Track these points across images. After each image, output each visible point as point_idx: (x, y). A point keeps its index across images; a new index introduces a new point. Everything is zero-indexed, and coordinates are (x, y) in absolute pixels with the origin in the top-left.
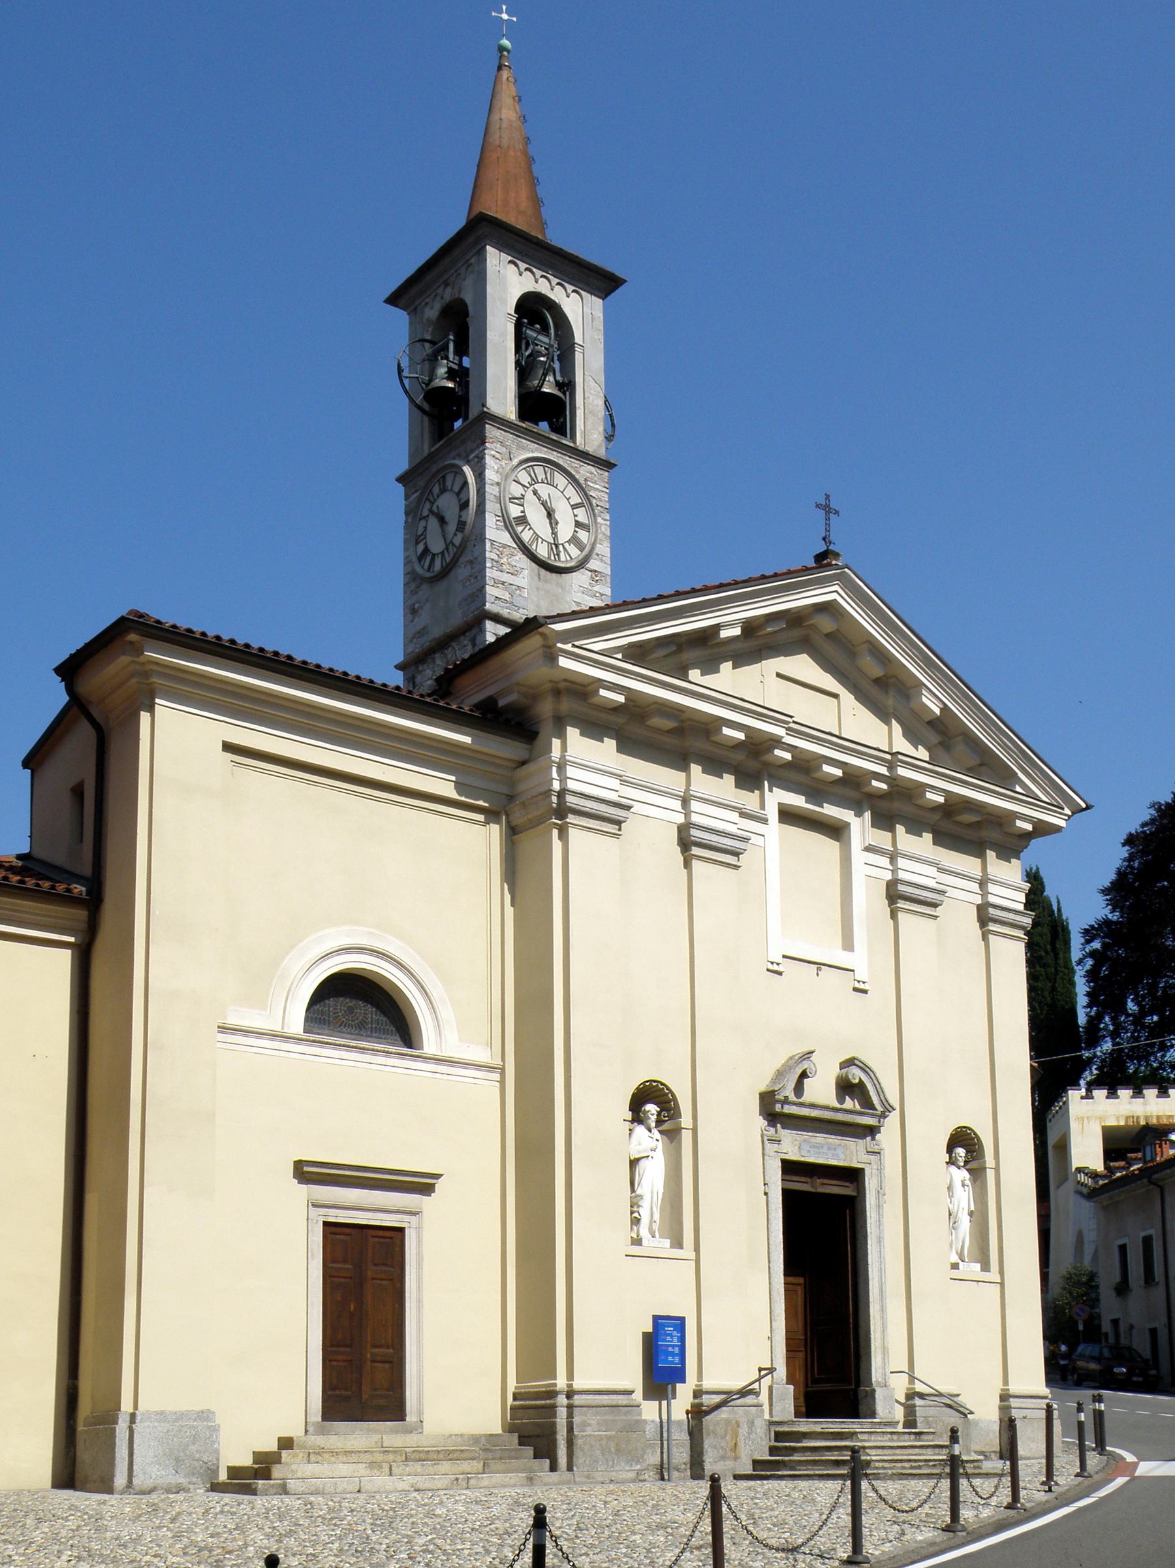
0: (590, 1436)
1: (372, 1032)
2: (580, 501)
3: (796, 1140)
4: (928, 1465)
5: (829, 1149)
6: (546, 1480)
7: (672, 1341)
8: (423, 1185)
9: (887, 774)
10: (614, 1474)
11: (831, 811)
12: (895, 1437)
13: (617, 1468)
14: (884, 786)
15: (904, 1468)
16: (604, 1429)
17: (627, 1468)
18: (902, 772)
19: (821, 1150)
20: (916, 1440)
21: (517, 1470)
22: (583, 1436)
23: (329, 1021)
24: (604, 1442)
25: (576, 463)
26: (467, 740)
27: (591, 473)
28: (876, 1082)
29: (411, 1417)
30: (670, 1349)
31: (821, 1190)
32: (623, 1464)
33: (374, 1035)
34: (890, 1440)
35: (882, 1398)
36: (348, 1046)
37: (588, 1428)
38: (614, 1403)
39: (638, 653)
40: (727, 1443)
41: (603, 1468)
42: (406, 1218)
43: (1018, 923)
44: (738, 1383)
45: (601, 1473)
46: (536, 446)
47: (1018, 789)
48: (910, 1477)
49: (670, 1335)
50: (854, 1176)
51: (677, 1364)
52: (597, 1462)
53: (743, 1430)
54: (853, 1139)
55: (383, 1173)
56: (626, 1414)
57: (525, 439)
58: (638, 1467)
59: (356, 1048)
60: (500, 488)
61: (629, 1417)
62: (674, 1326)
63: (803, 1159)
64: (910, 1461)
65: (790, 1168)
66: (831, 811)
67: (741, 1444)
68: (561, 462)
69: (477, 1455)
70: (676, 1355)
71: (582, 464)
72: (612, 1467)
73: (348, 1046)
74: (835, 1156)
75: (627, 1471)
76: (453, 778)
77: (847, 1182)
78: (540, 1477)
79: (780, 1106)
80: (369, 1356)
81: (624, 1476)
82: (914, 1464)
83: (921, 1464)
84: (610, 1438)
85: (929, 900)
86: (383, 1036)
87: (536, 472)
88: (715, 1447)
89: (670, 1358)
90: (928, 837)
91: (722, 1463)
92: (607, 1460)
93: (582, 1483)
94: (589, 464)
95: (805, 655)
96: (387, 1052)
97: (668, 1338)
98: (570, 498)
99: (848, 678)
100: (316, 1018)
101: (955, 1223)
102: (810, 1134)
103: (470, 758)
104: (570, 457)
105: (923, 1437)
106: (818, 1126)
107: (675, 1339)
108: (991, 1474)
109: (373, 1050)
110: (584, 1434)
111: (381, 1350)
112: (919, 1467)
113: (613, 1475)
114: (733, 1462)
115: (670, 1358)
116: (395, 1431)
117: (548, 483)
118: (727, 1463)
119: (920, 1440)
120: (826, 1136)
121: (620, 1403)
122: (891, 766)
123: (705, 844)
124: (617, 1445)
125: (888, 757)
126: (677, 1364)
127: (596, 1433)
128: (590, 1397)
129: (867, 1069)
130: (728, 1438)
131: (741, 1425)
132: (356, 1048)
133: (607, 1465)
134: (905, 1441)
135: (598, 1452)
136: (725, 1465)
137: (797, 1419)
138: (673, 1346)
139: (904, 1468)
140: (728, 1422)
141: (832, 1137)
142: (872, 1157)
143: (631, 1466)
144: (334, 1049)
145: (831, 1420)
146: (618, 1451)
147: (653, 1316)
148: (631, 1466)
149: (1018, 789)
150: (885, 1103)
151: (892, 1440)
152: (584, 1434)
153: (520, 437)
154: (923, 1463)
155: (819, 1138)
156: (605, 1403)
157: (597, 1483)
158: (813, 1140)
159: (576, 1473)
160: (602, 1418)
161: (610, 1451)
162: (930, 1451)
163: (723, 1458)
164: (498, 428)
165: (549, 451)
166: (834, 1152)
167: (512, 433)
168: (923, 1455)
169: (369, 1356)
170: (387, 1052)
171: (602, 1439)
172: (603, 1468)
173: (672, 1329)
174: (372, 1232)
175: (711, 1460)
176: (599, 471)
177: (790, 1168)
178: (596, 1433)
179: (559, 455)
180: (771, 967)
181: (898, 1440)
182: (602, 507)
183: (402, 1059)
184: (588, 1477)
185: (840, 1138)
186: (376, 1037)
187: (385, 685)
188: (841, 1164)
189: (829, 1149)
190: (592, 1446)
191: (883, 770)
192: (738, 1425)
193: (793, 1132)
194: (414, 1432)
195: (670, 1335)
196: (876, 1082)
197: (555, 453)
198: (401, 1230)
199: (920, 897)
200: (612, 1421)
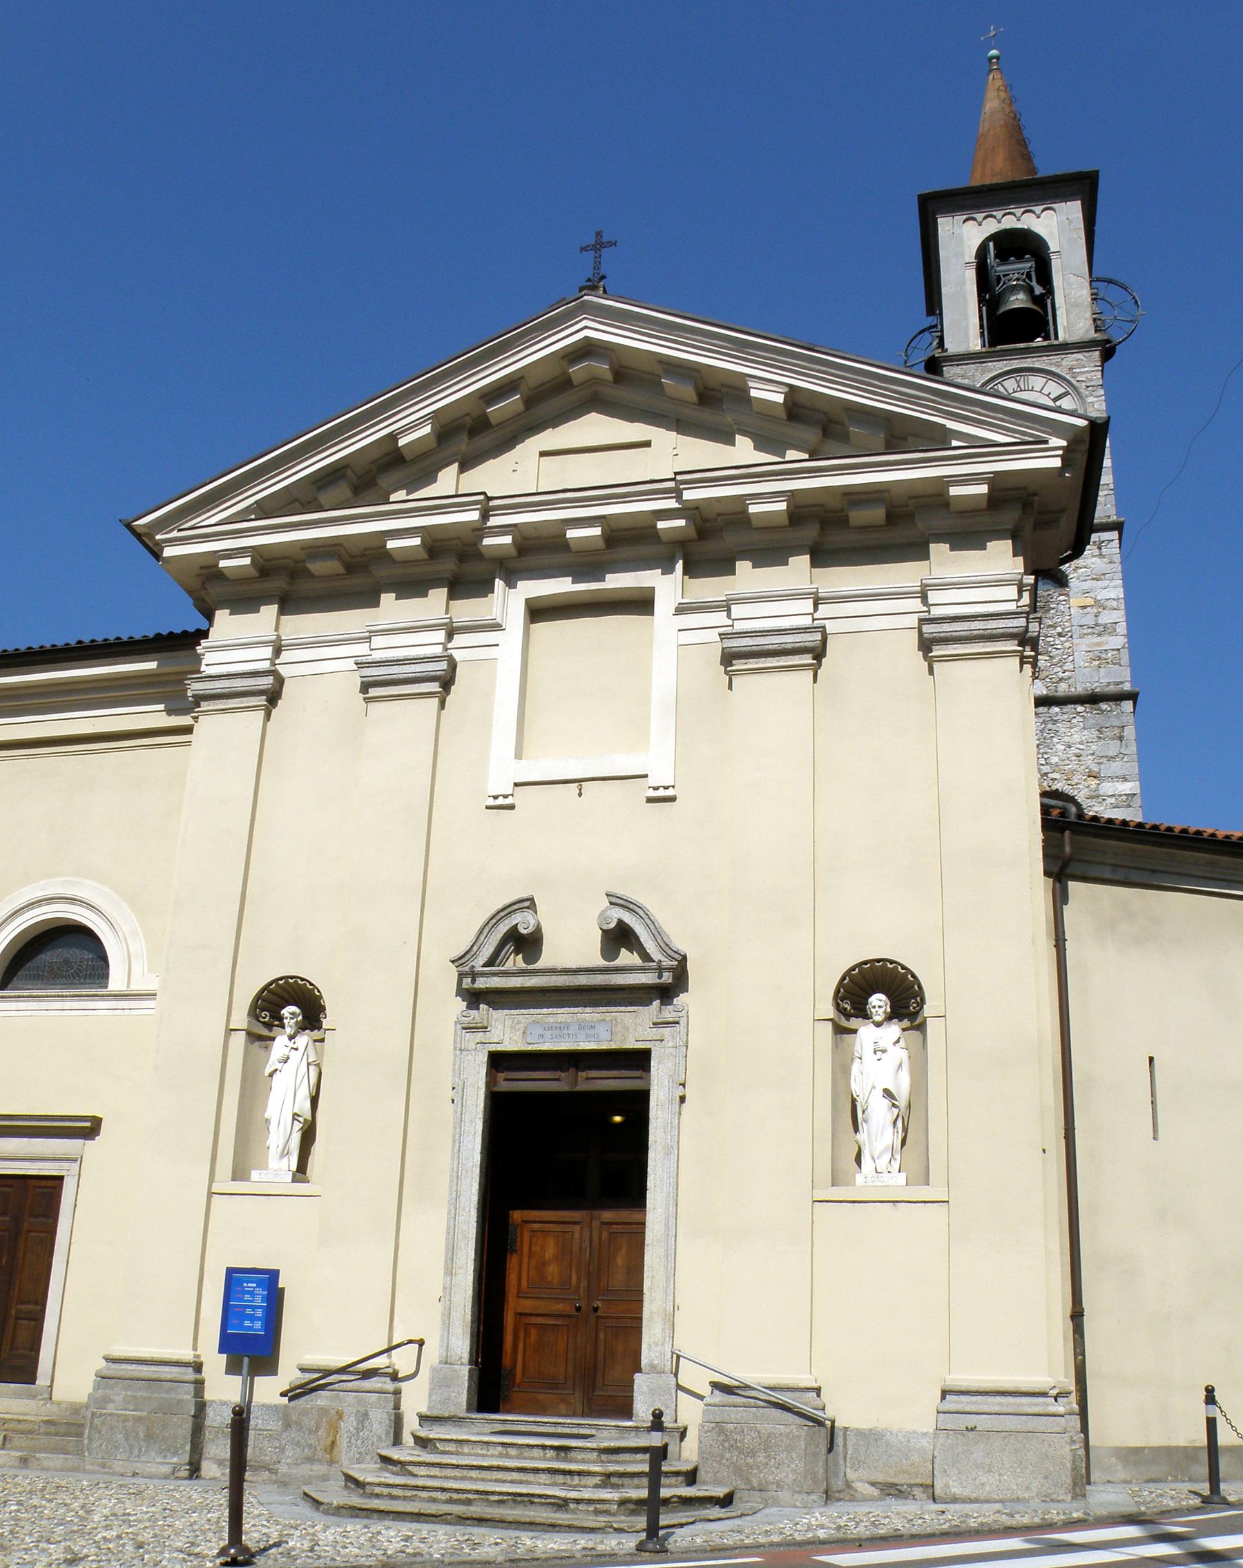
0: (111, 1415)
1: (85, 979)
2: (1064, 390)
3: (519, 1023)
4: (488, 1500)
5: (581, 1028)
6: (45, 1463)
7: (252, 1301)
8: (89, 1129)
9: (677, 505)
10: (139, 1465)
11: (618, 581)
12: (513, 1452)
13: (143, 1458)
14: (681, 523)
15: (434, 1500)
16: (131, 1408)
17: (159, 1460)
18: (688, 495)
19: (565, 1032)
20: (557, 1459)
21: (45, 1449)
22: (101, 1415)
23: (43, 975)
24: (130, 1424)
25: (1056, 359)
26: (152, 665)
27: (1078, 360)
28: (649, 922)
29: (42, 1380)
30: (249, 1311)
31: (583, 1086)
32: (153, 1454)
33: (88, 981)
34: (501, 1456)
35: (645, 1389)
36: (23, 997)
37: (110, 1406)
38: (155, 1376)
39: (264, 509)
40: (319, 1441)
41: (124, 1456)
42: (65, 1165)
43: (994, 632)
44: (346, 1359)
45: (121, 1463)
46: (1005, 362)
47: (955, 443)
48: (375, 1515)
49: (252, 1293)
50: (639, 1060)
51: (258, 1330)
52: (117, 1448)
53: (349, 1424)
54: (630, 1009)
55: (31, 1121)
56: (169, 1391)
57: (991, 362)
58: (175, 1460)
59: (30, 997)
60: (524, 412)
61: (173, 1396)
62: (260, 1284)
63: (530, 1048)
64: (443, 1490)
65: (499, 1061)
66: (618, 581)
67: (343, 1443)
68: (1037, 365)
69: (36, 1427)
70: (258, 1319)
71: (1063, 356)
72: (138, 1456)
73: (23, 997)
74: (597, 1038)
75: (159, 1463)
76: (162, 707)
77: (638, 1069)
78: (38, 1459)
79: (469, 980)
80: (13, 1312)
81: (154, 1470)
82: (455, 1496)
83: (471, 1496)
84: (139, 1420)
85: (789, 646)
86: (97, 981)
87: (1006, 386)
88: (298, 1444)
89: (247, 1323)
90: (801, 562)
91: (308, 1466)
92: (131, 1446)
93: (94, 1472)
94: (1073, 353)
95: (594, 413)
96: (62, 996)
97: (247, 1297)
98: (1049, 394)
99: (666, 416)
100: (34, 975)
101: (864, 1112)
102: (545, 1011)
103: (161, 684)
104: (1048, 356)
105: (573, 1454)
106: (558, 998)
107: (259, 1299)
108: (560, 1526)
109: (48, 997)
110: (104, 1411)
111: (29, 1307)
112: (469, 1502)
113: (138, 1467)
114: (326, 1467)
115: (247, 1323)
116: (17, 1396)
117: (1021, 391)
118: (314, 1467)
119: (565, 1460)
120: (576, 1010)
121: (163, 1376)
122: (679, 498)
123: (383, 681)
124: (148, 1429)
125: (671, 484)
126: (258, 1330)
127: (120, 1412)
128: (133, 1367)
129: (631, 906)
130: (322, 1433)
131: (345, 1418)
132: (30, 997)
133: (131, 1453)
134: (532, 1459)
135: (120, 1436)
136: (312, 1470)
137: (469, 1415)
138: (254, 1308)
139: (434, 1500)
140: (323, 1411)
141: (588, 1009)
142: (666, 1031)
143: (165, 1457)
144: (11, 1001)
145: (551, 1420)
146: (149, 1437)
147: (279, 1270)
148: (165, 1457)
149: (955, 443)
150: (666, 949)
151: (508, 1456)
152: (104, 1411)
153: (984, 362)
154: (476, 1496)
155: (563, 1015)
156: (142, 1375)
157: (114, 1474)
158: (551, 1019)
159: (87, 1459)
160: (134, 1394)
161: (137, 1437)
162: (543, 1478)
163: (310, 1460)
164: (958, 365)
165: (1022, 360)
166: (592, 1032)
167: (974, 363)
168: (528, 1483)
169: (13, 1312)
170: (62, 996)
171: (128, 1420)
172: (124, 1456)
173: (255, 1285)
174: (33, 1182)
175: (289, 1461)
176: (1086, 354)
177: (499, 1061)
178: (120, 1412)
179: (1035, 359)
180: (491, 802)
181: (518, 1457)
182: (1093, 386)
183: (80, 1001)
184: (103, 1466)
185: (604, 1009)
186: (89, 984)
187: (80, 642)
188: (604, 1046)
189: (581, 1028)
190: (112, 1428)
191: (672, 504)
192: (340, 1415)
193: (513, 1012)
194: (39, 1397)
195: (252, 1293)
196: (649, 922)
197: (1029, 360)
198: (60, 1179)
199: (770, 647)
200: (145, 1399)
